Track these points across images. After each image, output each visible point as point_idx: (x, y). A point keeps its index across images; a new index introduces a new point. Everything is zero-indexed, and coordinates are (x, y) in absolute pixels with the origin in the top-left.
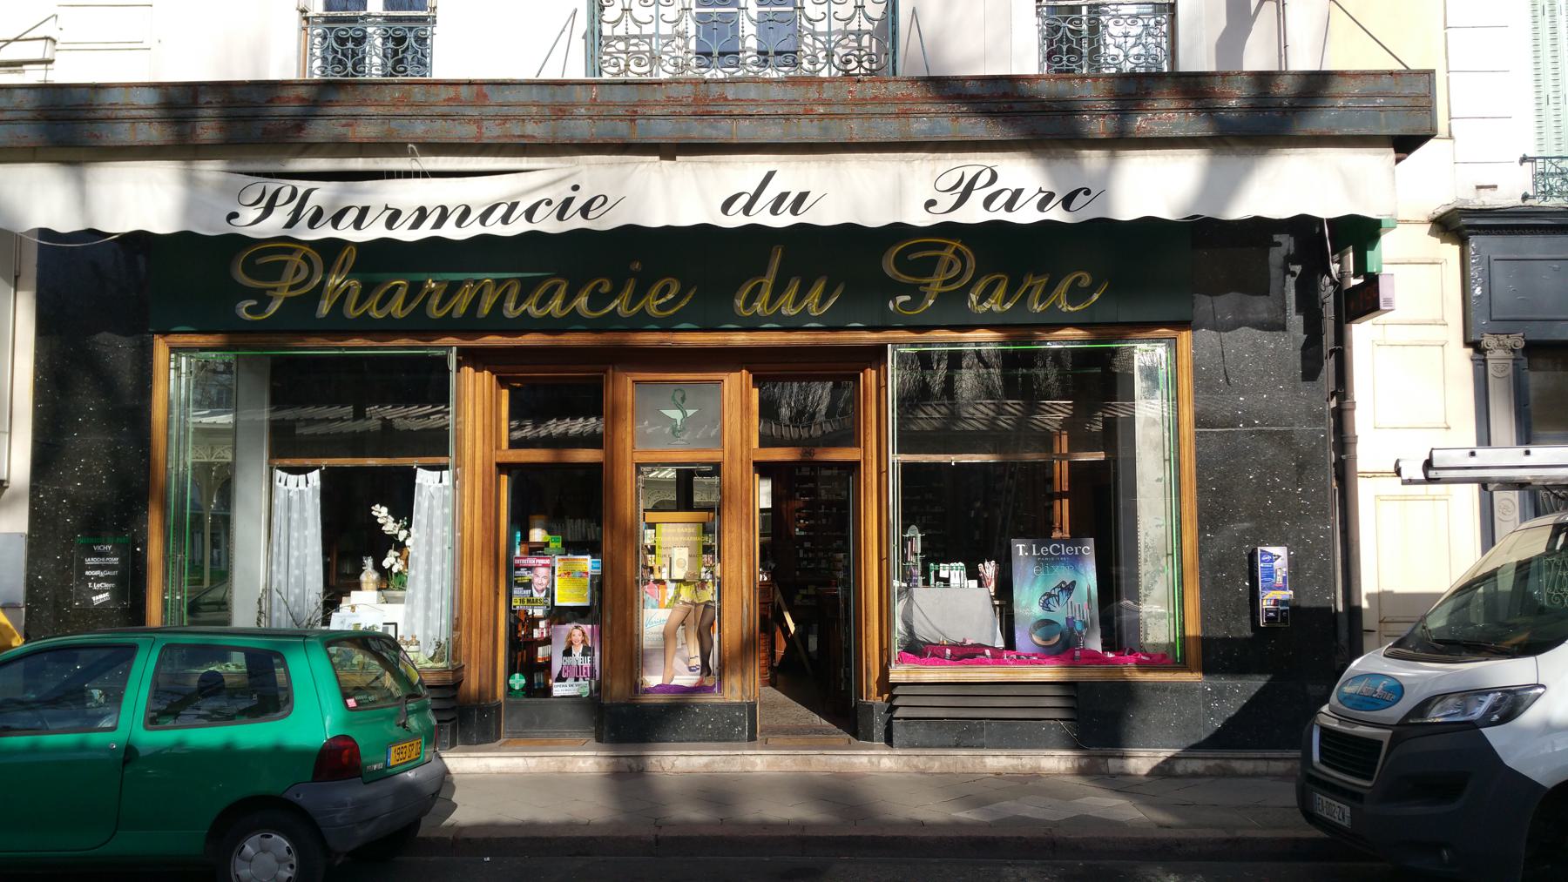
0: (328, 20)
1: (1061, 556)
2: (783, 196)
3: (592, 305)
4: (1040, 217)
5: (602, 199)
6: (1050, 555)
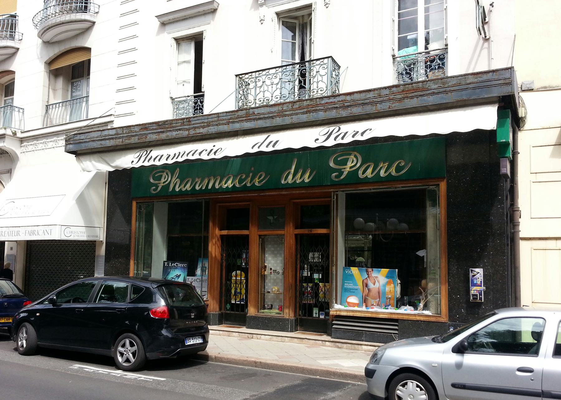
0: (195, 97)
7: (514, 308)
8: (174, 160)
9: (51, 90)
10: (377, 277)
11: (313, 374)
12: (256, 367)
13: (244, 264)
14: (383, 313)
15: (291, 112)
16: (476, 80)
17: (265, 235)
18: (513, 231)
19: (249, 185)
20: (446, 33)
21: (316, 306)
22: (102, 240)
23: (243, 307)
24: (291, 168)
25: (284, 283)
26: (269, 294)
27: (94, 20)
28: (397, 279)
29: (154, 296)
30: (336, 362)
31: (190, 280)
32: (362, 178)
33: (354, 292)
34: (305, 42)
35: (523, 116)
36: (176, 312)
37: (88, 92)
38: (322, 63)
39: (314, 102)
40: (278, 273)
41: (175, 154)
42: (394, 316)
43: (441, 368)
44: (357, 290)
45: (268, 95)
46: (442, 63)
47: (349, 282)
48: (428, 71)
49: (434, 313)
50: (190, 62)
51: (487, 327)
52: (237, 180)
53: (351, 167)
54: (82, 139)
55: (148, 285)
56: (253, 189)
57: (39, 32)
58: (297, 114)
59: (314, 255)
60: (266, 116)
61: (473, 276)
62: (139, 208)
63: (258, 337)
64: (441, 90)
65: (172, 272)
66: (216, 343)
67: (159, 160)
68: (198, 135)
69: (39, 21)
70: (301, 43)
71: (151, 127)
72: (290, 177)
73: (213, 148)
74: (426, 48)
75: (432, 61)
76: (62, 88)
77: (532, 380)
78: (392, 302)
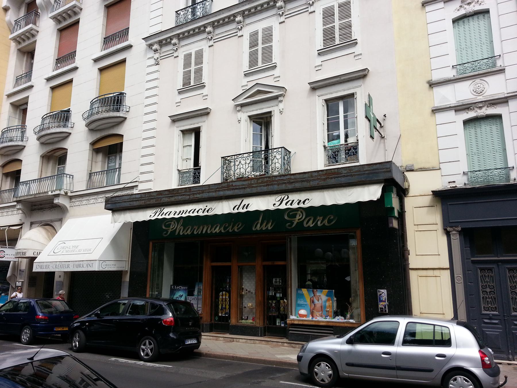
0: (194, 169)
2: (245, 205)
5: (211, 209)
7: (408, 316)
8: (180, 216)
10: (320, 296)
11: (271, 364)
12: (233, 360)
13: (228, 287)
14: (323, 322)
15: (257, 185)
16: (369, 169)
17: (242, 266)
18: (404, 264)
19: (230, 231)
20: (357, 133)
21: (278, 317)
24: (259, 219)
25: (256, 300)
26: (245, 309)
27: (126, 117)
28: (334, 297)
30: (288, 356)
31: (190, 299)
33: (304, 307)
35: (407, 187)
36: (179, 322)
37: (120, 164)
40: (252, 293)
41: (181, 211)
42: (330, 324)
43: (340, 353)
44: (306, 305)
45: (242, 170)
47: (301, 299)
48: (347, 156)
49: (357, 321)
50: (192, 146)
51: (367, 327)
52: (223, 228)
53: (299, 220)
54: (117, 200)
56: (234, 233)
58: (260, 186)
59: (276, 280)
60: (240, 187)
61: (380, 295)
62: (154, 247)
63: (237, 341)
66: (207, 345)
67: (169, 215)
68: (196, 198)
70: (266, 134)
72: (259, 225)
73: (206, 208)
74: (346, 141)
75: (349, 150)
76: (101, 161)
77: (391, 360)
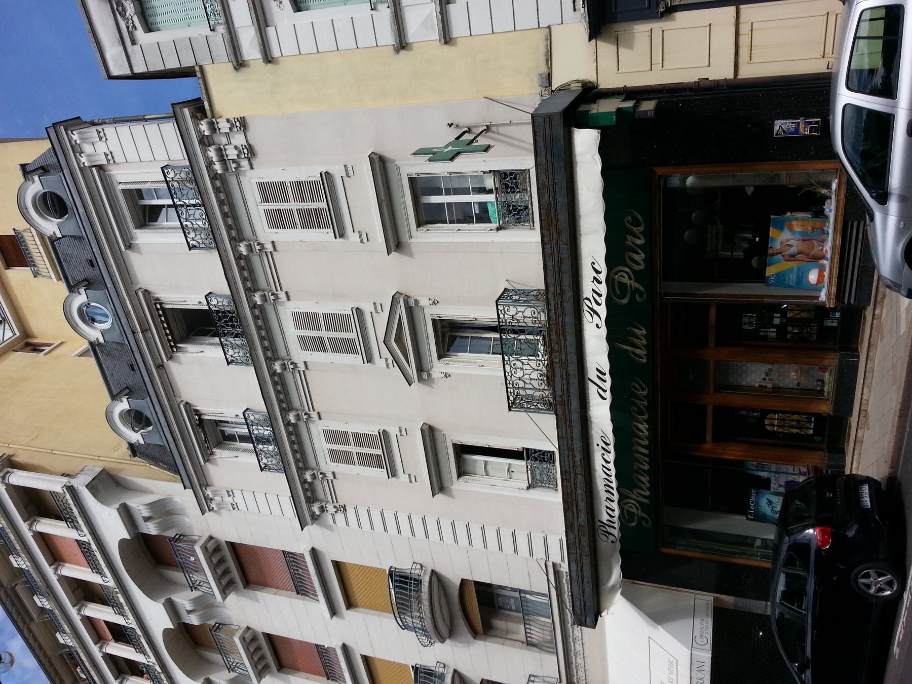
0: (528, 459)
1: (755, 501)
2: (598, 376)
3: (639, 225)
4: (604, 305)
5: (602, 438)
6: (755, 506)
9: (508, 637)
10: (781, 243)
13: (756, 414)
14: (834, 240)
15: (563, 353)
16: (543, 153)
19: (646, 403)
20: (477, 172)
22: (713, 598)
23: (820, 418)
24: (627, 351)
27: (430, 570)
28: (784, 216)
29: (798, 541)
32: (644, 265)
33: (803, 272)
34: (471, 325)
35: (580, 84)
38: (503, 312)
39: (553, 326)
42: (839, 227)
44: (799, 269)
45: (535, 375)
46: (510, 175)
47: (787, 279)
48: (518, 190)
52: (639, 417)
53: (630, 278)
54: (579, 605)
55: (785, 548)
57: (440, 641)
58: (566, 347)
59: (746, 324)
60: (565, 382)
64: (551, 190)
65: (762, 511)
69: (427, 639)
71: (570, 519)
72: (638, 351)
73: (600, 447)
75: (507, 186)
78: (818, 225)
